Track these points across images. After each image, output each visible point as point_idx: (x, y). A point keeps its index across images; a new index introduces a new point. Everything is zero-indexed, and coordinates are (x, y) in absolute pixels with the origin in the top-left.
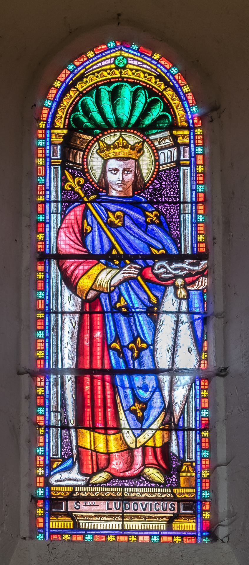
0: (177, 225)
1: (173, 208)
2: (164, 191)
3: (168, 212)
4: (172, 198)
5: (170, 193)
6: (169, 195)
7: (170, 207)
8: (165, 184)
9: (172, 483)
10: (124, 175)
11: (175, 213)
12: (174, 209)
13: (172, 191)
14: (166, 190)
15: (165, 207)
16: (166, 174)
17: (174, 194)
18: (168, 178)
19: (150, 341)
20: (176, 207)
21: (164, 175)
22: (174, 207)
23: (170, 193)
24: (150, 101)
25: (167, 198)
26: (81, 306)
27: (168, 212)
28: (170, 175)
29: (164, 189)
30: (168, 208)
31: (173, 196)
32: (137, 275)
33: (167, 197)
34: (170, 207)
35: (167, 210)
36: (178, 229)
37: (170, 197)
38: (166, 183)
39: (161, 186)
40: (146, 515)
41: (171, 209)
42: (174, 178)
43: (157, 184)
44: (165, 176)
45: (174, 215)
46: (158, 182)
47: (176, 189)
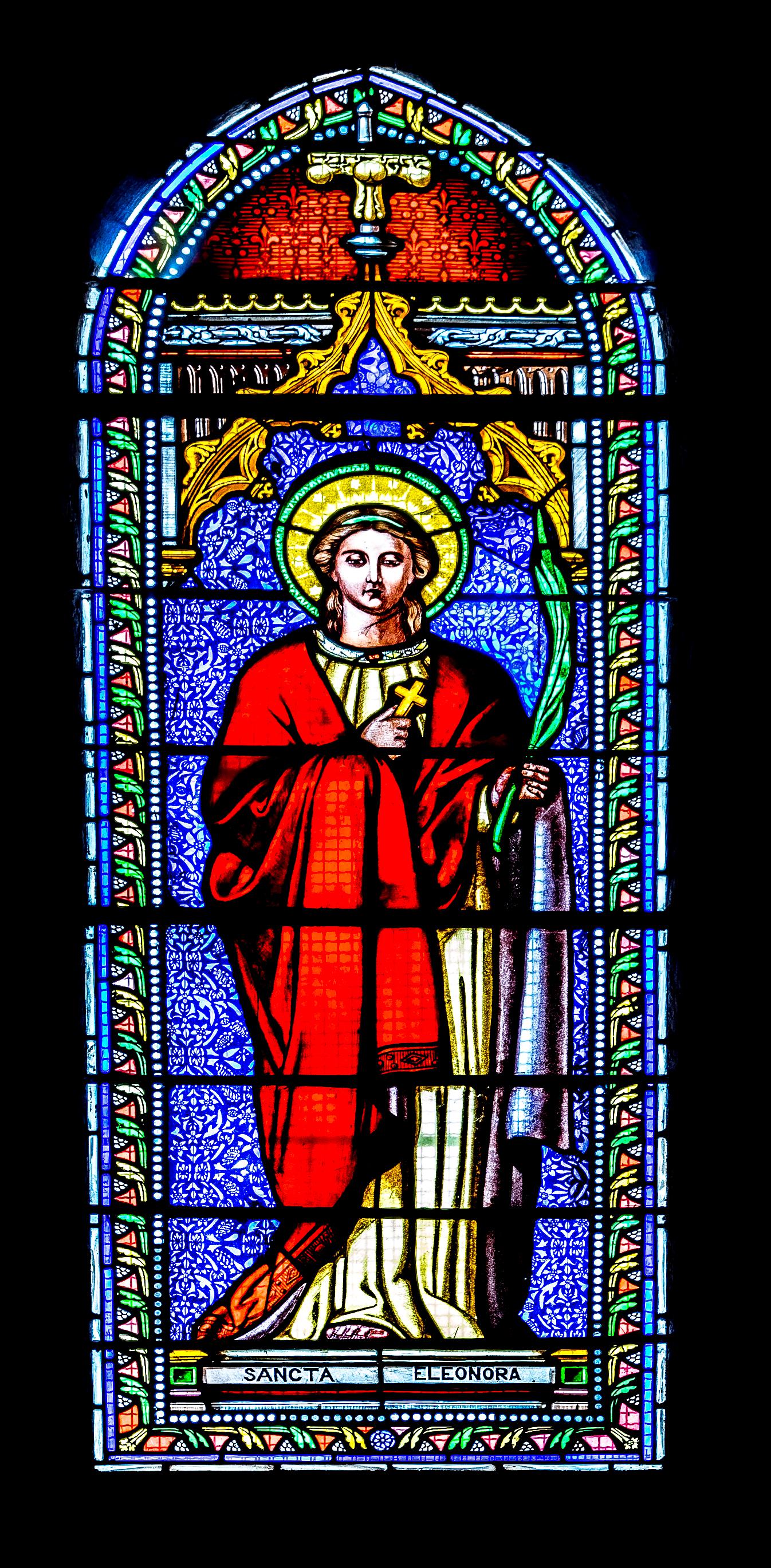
1: (182, 992)
2: (211, 1038)
3: (199, 1261)
4: (185, 1298)
5: (194, 1033)
6: (196, 1027)
10: (383, 567)
13: (184, 943)
14: (204, 1041)
15: (208, 1274)
16: (204, 1272)
23: (194, 1033)
25: (200, 1019)
26: (445, 1013)
29: (211, 1045)
31: (183, 1303)
35: (201, 1267)
37: (192, 1022)
38: (206, 1061)
40: (239, 1458)
43: (233, 1058)
47: (174, 1044)
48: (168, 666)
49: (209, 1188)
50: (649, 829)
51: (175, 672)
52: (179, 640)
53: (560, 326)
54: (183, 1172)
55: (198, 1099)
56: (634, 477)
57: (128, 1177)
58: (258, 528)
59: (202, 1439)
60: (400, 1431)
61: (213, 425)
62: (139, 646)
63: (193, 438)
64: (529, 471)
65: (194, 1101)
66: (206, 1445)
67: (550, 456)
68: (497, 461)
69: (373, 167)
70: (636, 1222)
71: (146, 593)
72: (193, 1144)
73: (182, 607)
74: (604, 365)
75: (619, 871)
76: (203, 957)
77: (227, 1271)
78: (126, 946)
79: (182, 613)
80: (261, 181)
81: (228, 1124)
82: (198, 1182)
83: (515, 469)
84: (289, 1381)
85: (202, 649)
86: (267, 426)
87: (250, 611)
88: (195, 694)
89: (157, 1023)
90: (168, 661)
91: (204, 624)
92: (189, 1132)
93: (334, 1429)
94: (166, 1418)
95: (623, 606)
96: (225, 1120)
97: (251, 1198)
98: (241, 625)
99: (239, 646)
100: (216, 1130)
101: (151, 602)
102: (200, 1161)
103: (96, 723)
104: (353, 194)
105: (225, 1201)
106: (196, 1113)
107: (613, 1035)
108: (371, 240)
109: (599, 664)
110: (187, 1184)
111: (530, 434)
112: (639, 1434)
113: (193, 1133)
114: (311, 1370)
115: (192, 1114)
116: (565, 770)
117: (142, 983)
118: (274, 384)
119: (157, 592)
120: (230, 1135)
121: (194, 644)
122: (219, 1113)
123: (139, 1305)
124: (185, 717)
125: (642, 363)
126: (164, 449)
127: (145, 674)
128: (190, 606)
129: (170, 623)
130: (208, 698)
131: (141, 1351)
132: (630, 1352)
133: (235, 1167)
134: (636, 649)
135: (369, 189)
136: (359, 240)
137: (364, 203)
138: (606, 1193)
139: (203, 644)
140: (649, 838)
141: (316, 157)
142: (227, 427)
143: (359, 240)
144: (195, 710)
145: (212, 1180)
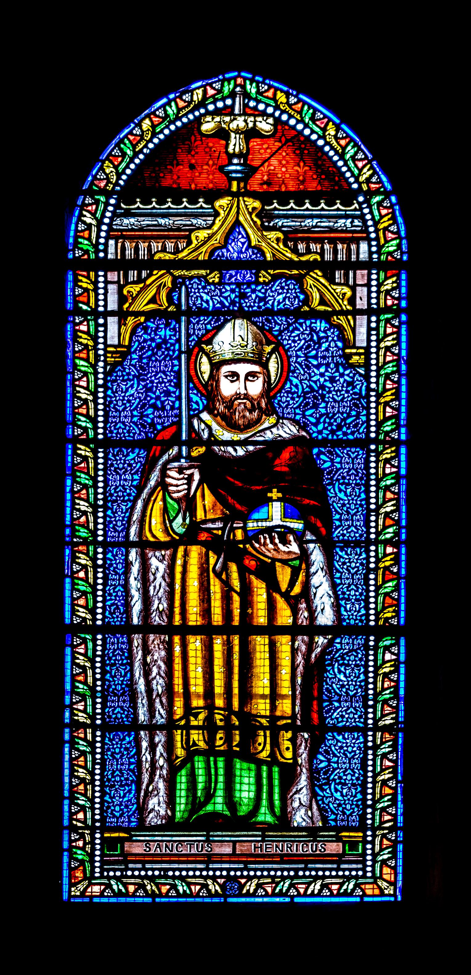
0: (360, 532)
7: (349, 500)
9: (347, 721)
15: (338, 682)
18: (345, 567)
20: (356, 801)
22: (356, 500)
24: (308, 504)
28: (348, 503)
30: (343, 684)
32: (169, 467)
33: (340, 783)
34: (349, 616)
36: (362, 720)
39: (332, 465)
44: (340, 563)
45: (355, 514)
46: (327, 459)
48: (108, 675)
51: (114, 515)
52: (118, 496)
54: (114, 580)
55: (123, 492)
56: (395, 336)
57: (82, 482)
58: (158, 393)
59: (121, 887)
61: (139, 275)
63: (127, 283)
66: (124, 891)
71: (96, 543)
72: (118, 684)
73: (118, 639)
77: (309, 374)
78: (81, 579)
82: (123, 423)
85: (130, 380)
86: (172, 274)
87: (160, 357)
88: (126, 408)
89: (101, 494)
90: (107, 793)
91: (132, 365)
92: (116, 512)
93: (201, 881)
94: (101, 873)
95: (388, 448)
96: (139, 385)
98: (155, 365)
99: (153, 378)
101: (100, 550)
106: (122, 381)
108: (239, 168)
109: (373, 483)
110: (117, 424)
111: (332, 281)
113: (119, 513)
115: (119, 381)
116: (348, 724)
117: (91, 575)
118: (177, 251)
121: (126, 377)
123: (87, 535)
124: (120, 421)
127: (96, 404)
128: (122, 760)
129: (112, 485)
130: (134, 410)
131: (86, 832)
133: (145, 413)
134: (394, 390)
135: (238, 136)
137: (235, 145)
139: (131, 377)
144: (126, 417)
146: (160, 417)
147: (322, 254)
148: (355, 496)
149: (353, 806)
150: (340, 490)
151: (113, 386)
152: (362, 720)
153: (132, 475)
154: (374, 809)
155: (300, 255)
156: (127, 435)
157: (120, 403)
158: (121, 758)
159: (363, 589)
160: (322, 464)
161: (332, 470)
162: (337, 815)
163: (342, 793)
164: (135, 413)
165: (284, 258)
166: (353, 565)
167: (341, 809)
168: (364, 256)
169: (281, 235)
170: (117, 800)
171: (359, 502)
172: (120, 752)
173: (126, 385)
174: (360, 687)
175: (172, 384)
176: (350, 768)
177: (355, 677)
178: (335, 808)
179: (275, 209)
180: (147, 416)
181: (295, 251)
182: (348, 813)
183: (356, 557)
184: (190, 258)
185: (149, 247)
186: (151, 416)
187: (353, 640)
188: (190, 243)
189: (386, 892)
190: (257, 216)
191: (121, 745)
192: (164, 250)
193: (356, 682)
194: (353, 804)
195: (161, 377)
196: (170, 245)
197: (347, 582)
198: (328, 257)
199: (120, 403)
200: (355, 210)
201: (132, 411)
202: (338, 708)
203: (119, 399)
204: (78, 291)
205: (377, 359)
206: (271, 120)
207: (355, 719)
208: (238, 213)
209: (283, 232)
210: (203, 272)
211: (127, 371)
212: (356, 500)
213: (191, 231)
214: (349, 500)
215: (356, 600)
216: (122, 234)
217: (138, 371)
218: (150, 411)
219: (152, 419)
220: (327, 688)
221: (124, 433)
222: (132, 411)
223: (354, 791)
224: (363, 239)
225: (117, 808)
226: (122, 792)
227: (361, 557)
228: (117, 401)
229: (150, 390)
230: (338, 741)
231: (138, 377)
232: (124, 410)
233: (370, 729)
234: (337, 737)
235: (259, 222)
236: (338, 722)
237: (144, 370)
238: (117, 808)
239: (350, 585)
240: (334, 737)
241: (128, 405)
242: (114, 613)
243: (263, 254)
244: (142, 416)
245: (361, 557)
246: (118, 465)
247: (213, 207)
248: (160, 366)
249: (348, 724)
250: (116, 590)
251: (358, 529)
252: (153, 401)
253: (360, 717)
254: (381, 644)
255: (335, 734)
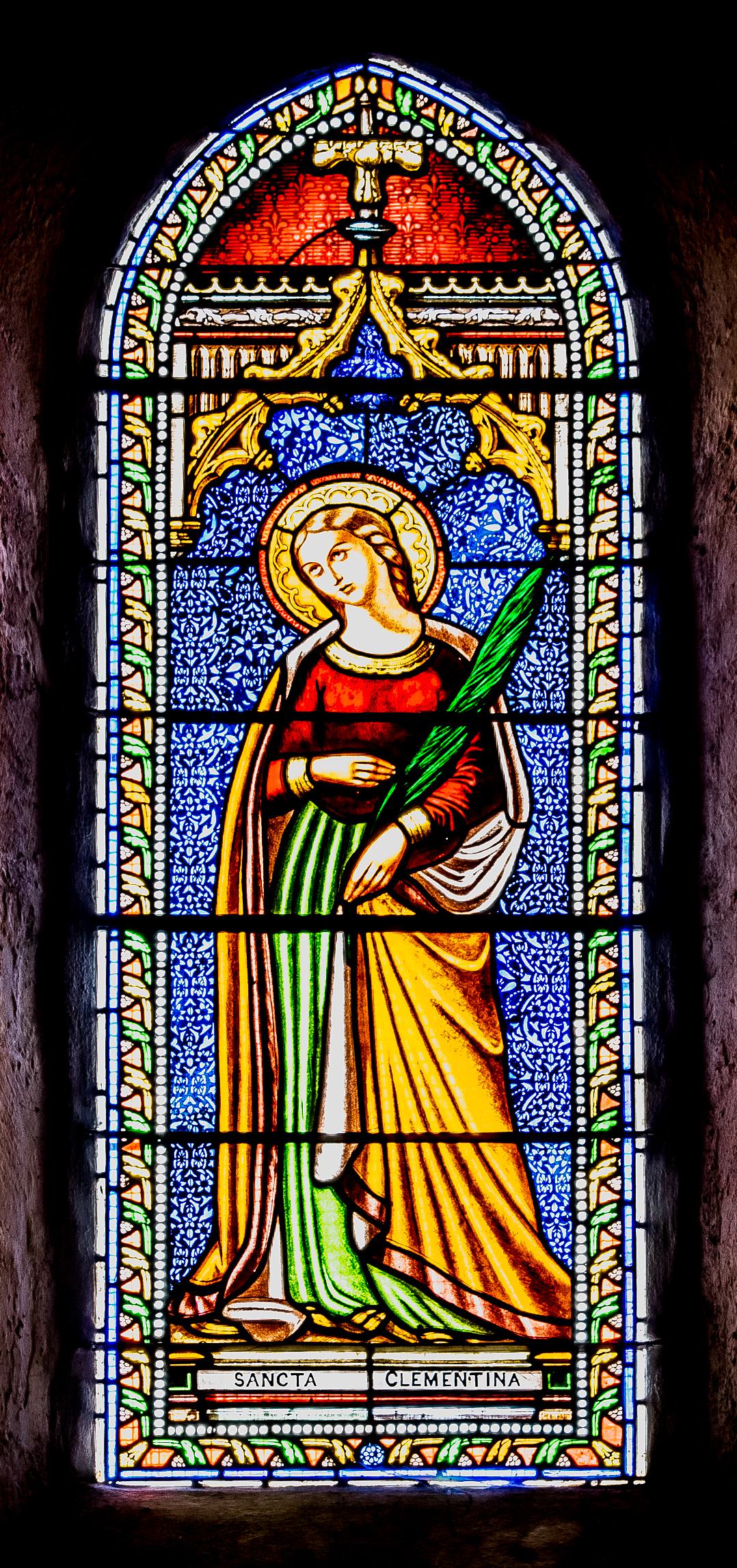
0: (560, 893)
8: (531, 983)
9: (542, 906)
11: (557, 685)
12: (554, 846)
14: (534, 1000)
17: (554, 1011)
18: (538, 963)
19: (373, 1302)
21: (526, 954)
22: (556, 1047)
27: (539, 1062)
29: (527, 995)
34: (545, 1047)
36: (565, 904)
37: (544, 1020)
39: (519, 988)
41: (545, 673)
42: (553, 756)
44: (530, 957)
46: (510, 977)
49: (206, 693)
50: (626, 981)
53: (540, 304)
55: (195, 1179)
58: (248, 637)
60: (388, 1442)
62: (148, 977)
64: (516, 447)
65: (190, 1011)
67: (534, 431)
68: (487, 435)
69: (369, 152)
70: (615, 1354)
74: (587, 1224)
75: (600, 1119)
76: (531, 703)
79: (190, 1158)
80: (271, 170)
81: (222, 529)
82: (196, 686)
83: (502, 444)
84: (276, 1387)
88: (199, 661)
90: (175, 1207)
91: (210, 589)
92: (185, 832)
96: (219, 524)
97: (245, 702)
100: (212, 533)
102: (195, 863)
103: (110, 362)
104: (353, 180)
105: (220, 706)
107: (592, 596)
110: (185, 688)
111: (514, 407)
112: (621, 1449)
114: (298, 1375)
116: (544, 910)
119: (168, 1139)
120: (223, 540)
122: (214, 615)
124: (190, 684)
125: (620, 437)
126: (173, 421)
132: (609, 575)
136: (356, 226)
138: (586, 900)
140: (626, 991)
141: (321, 145)
142: (232, 400)
143: (356, 226)
145: (208, 685)
146: (251, 677)
147: (496, 366)
148: (553, 659)
149: (556, 676)
150: (532, 1031)
151: (180, 623)
152: (565, 904)
153: (207, 767)
154: (589, 1227)
155: (464, 367)
156: (199, 905)
157: (189, 851)
158: (196, 975)
159: (566, 1001)
160: (503, 986)
161: (519, 996)
162: (531, 690)
163: (539, 1034)
164: (214, 670)
165: (443, 375)
166: (550, 960)
167: (537, 680)
168: (561, 370)
169: (434, 335)
170: (190, 640)
171: (559, 843)
172: (194, 966)
173: (199, 821)
174: (564, 1056)
175: (270, 621)
176: (549, 784)
177: (555, 1040)
178: (528, 678)
179: (428, 293)
180: (232, 675)
181: (456, 360)
182: (548, 687)
183: (555, 946)
184: (298, 374)
185: (238, 357)
186: (238, 676)
187: (549, 707)
188: (297, 350)
189: (608, 1463)
190: (396, 303)
191: (195, 743)
192: (259, 362)
193: (555, 840)
194: (555, 672)
195: (252, 512)
196: (268, 355)
197: (541, 989)
198: (506, 371)
199: (191, 653)
200: (549, 293)
201: (208, 666)
202: (529, 883)
203: (190, 1227)
204: (126, 1091)
205: (584, 872)
206: (418, 148)
207: (555, 902)
208: (368, 301)
209: (438, 329)
210: (316, 397)
211: (202, 599)
212: (555, 666)
213: (298, 331)
214: (543, 839)
215: (556, 812)
216: (195, 336)
217: (218, 599)
218: (236, 666)
219: (240, 681)
220: (513, 1060)
221: (195, 903)
222: (208, 666)
223: (557, 823)
224: (560, 341)
225: (191, 653)
226: (197, 1206)
227: (561, 946)
228: (185, 848)
229: (235, 631)
230: (530, 946)
231: (218, 610)
232: (195, 863)
233: (582, 1135)
234: (529, 939)
235: (400, 314)
236: (529, 908)
237: (227, 500)
238: (190, 1233)
239: (545, 995)
240: (524, 939)
241: (203, 656)
242: (185, 944)
243: (407, 367)
244: (224, 675)
245: (561, 946)
246: (185, 751)
247: (331, 292)
248: (251, 592)
249: (544, 910)
250: (185, 1103)
251: (557, 889)
252: (240, 650)
253: (562, 899)
254: (592, 944)
255: (526, 934)
